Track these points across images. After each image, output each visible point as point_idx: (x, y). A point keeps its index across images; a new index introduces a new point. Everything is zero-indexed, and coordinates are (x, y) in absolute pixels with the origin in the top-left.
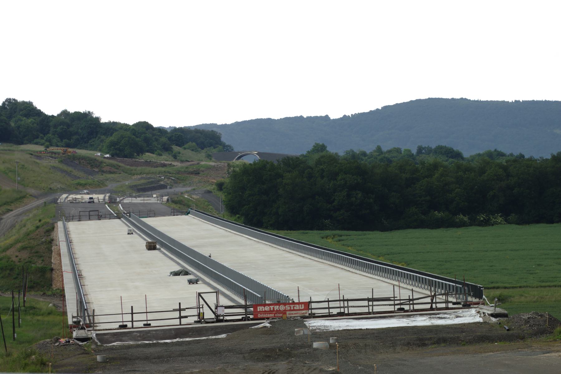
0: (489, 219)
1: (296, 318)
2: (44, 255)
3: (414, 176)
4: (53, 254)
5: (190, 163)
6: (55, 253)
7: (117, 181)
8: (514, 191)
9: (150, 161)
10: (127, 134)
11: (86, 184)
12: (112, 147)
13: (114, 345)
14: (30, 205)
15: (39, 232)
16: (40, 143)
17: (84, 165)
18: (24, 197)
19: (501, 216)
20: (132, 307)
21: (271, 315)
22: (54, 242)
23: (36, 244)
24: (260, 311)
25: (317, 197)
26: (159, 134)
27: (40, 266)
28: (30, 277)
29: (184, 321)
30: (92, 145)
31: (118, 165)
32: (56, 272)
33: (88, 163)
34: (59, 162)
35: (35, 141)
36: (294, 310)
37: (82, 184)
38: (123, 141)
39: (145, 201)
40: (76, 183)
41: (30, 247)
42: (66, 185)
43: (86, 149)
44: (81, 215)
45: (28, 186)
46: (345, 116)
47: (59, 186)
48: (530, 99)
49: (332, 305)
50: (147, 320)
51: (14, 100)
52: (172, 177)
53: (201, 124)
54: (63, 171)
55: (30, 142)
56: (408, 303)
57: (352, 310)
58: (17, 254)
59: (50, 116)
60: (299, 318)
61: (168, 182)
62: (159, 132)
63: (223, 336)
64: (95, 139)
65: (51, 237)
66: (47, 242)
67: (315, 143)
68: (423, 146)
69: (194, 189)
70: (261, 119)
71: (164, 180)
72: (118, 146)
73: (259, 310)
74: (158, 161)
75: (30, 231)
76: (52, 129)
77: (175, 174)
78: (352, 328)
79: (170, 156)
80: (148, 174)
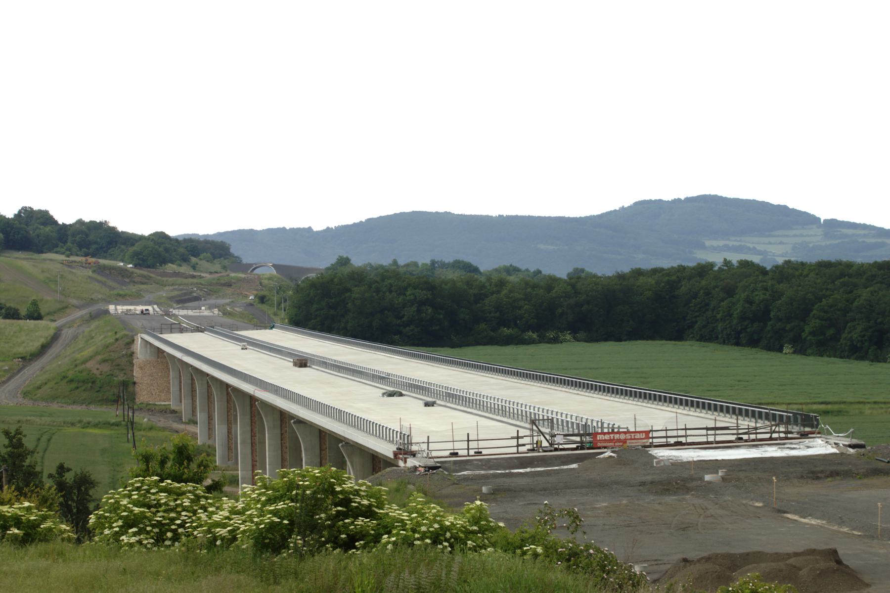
0: (558, 336)
1: (637, 447)
2: (125, 368)
3: (482, 292)
4: (135, 366)
5: (219, 275)
8: (582, 309)
11: (125, 295)
13: (464, 475)
18: (66, 307)
19: (569, 334)
20: (468, 434)
21: (611, 444)
24: (600, 440)
26: (176, 244)
29: (521, 449)
30: (111, 255)
34: (92, 272)
35: (55, 250)
36: (635, 439)
46: (328, 228)
47: (100, 297)
48: (514, 214)
49: (670, 433)
50: (478, 449)
51: (30, 208)
55: (50, 250)
56: (755, 432)
57: (690, 440)
58: (97, 366)
59: (68, 225)
60: (640, 447)
63: (574, 466)
64: (114, 249)
65: (132, 349)
68: (436, 260)
69: (232, 302)
70: (243, 230)
73: (598, 439)
76: (70, 238)
78: (708, 459)
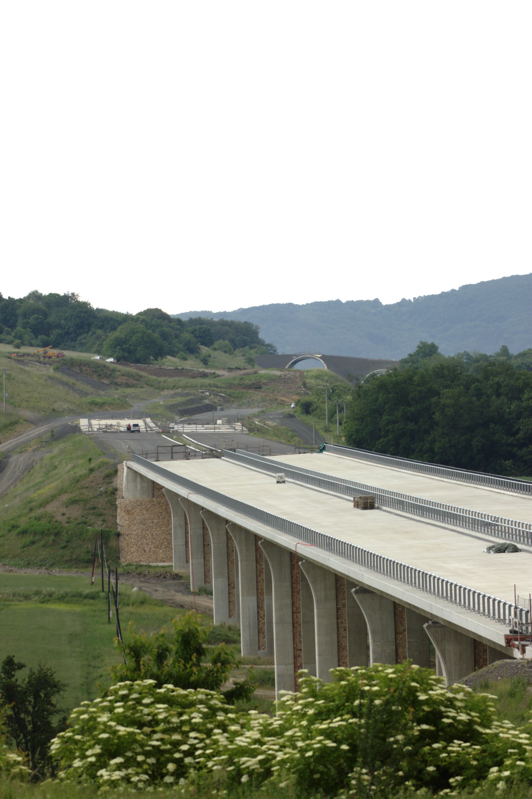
2: (104, 512)
6: (121, 509)
7: (141, 399)
9: (183, 369)
10: (140, 327)
11: (104, 404)
12: (119, 347)
14: (25, 435)
15: (94, 477)
16: (5, 340)
17: (87, 374)
18: (16, 423)
22: (119, 492)
23: (91, 496)
25: (492, 425)
26: (178, 327)
27: (99, 529)
28: (85, 546)
30: (82, 344)
31: (138, 375)
32: (124, 538)
33: (93, 371)
37: (99, 403)
38: (134, 337)
39: (216, 430)
40: (89, 403)
41: (82, 501)
42: (75, 404)
43: (73, 350)
44: (159, 452)
45: (20, 406)
46: (404, 300)
47: (65, 406)
52: (220, 392)
53: (188, 311)
54: (65, 384)
58: (64, 510)
61: (216, 400)
62: (178, 324)
65: (114, 484)
66: (109, 492)
67: (421, 342)
69: (263, 412)
71: (210, 398)
72: (127, 346)
74: (195, 369)
75: (80, 476)
76: (20, 320)
77: (225, 388)
79: (198, 361)
80: (185, 387)
